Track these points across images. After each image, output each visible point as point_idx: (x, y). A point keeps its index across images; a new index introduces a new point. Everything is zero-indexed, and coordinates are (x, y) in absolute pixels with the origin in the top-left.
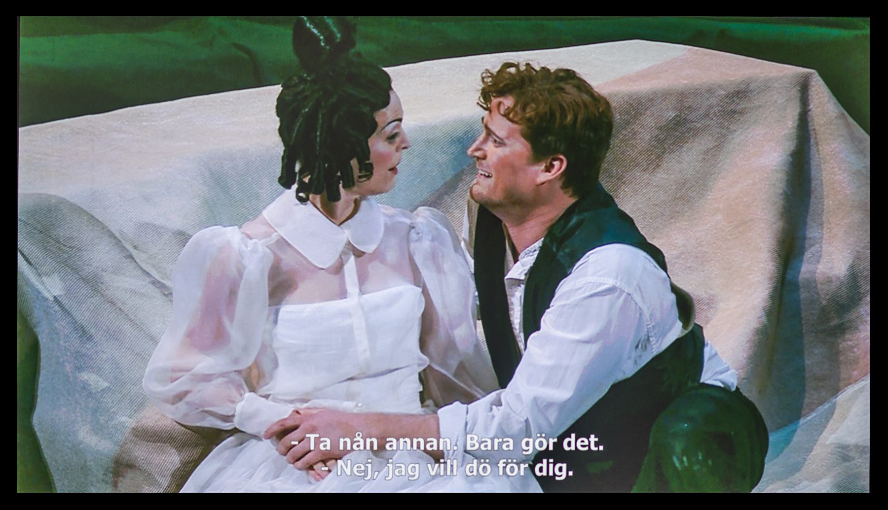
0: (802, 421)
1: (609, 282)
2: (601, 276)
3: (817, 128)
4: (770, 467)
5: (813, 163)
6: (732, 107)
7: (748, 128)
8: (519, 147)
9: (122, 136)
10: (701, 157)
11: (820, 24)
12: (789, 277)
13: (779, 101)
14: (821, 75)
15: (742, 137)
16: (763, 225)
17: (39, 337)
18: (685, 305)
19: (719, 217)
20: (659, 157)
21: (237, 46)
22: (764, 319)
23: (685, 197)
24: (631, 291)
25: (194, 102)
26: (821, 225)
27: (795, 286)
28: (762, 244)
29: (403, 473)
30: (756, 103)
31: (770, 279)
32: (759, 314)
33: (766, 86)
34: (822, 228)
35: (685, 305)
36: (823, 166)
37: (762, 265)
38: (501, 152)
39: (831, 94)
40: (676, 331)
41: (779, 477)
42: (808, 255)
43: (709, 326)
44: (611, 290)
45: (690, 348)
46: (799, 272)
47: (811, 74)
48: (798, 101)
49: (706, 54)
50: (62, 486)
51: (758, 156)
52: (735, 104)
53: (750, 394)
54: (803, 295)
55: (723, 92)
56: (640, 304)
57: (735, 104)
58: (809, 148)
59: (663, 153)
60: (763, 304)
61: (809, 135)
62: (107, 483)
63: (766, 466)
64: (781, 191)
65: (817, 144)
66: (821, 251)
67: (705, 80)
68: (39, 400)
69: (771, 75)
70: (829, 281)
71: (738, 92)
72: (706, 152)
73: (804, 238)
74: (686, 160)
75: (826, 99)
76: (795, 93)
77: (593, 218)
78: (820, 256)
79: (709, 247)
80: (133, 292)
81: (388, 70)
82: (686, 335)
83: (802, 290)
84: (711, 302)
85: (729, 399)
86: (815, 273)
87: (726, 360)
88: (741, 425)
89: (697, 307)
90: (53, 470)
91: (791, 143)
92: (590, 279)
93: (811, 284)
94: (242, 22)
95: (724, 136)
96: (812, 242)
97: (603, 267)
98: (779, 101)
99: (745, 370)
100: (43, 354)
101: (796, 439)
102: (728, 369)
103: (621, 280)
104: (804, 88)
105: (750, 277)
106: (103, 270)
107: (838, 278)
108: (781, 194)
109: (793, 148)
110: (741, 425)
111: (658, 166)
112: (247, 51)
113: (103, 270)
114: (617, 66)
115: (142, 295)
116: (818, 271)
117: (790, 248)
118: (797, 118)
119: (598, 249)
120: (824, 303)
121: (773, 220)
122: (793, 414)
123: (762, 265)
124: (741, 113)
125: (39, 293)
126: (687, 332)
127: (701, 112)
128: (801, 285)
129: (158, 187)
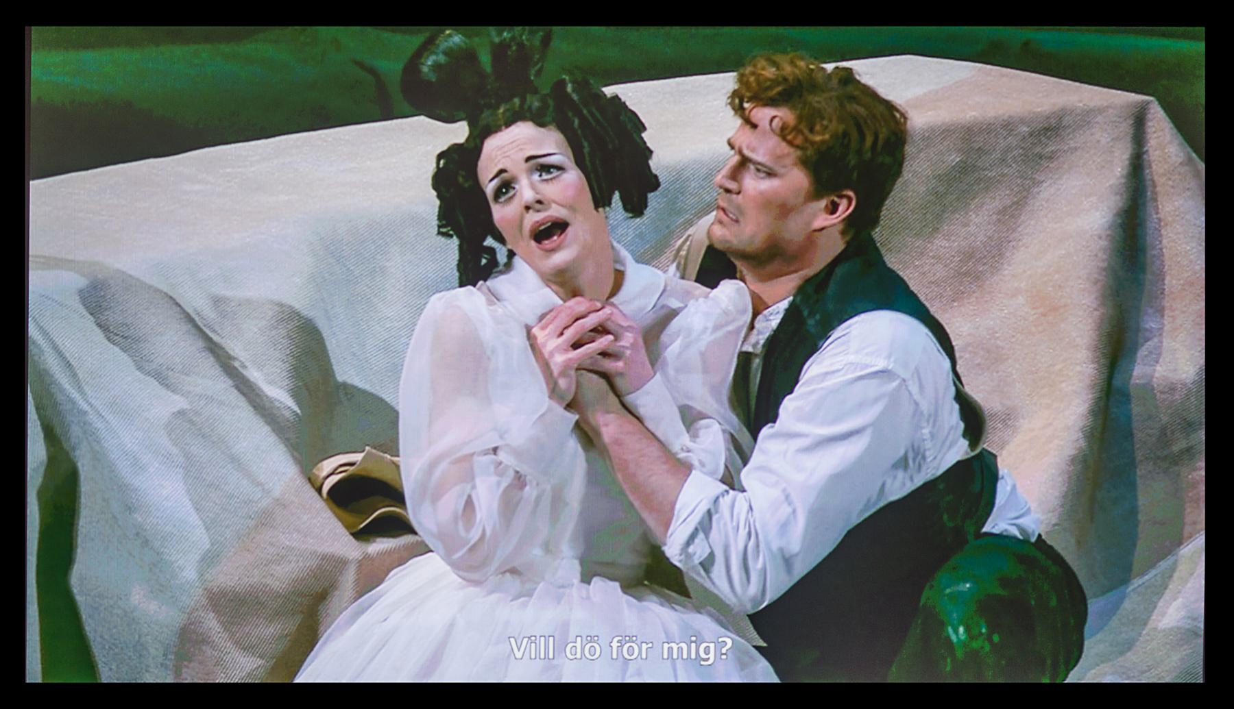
0: (1136, 582)
1: (881, 364)
2: (867, 354)
3: (1156, 178)
4: (1093, 645)
5: (1151, 225)
6: (1038, 150)
7: (1060, 178)
8: (797, 179)
9: (197, 187)
10: (995, 217)
11: (1164, 35)
12: (1117, 382)
13: (1103, 141)
14: (1160, 103)
15: (1052, 190)
16: (1081, 313)
17: (79, 465)
18: (973, 420)
19: (1021, 300)
20: (939, 218)
21: (360, 65)
22: (1082, 443)
23: (975, 269)
24: (904, 374)
25: (298, 139)
26: (1161, 311)
27: (1126, 396)
28: (1078, 339)
29: (578, 656)
30: (1072, 144)
31: (1093, 387)
32: (1075, 437)
33: (1085, 118)
34: (1163, 316)
35: (973, 420)
36: (1163, 232)
37: (1078, 368)
38: (766, 185)
39: (1175, 131)
40: (959, 450)
41: (1103, 659)
42: (1142, 352)
43: (1004, 452)
44: (883, 373)
45: (975, 480)
46: (1131, 375)
47: (1148, 103)
48: (1129, 138)
49: (1003, 75)
50: (108, 674)
51: (1073, 216)
52: (1043, 140)
53: (1064, 546)
54: (1136, 409)
55: (1025, 129)
56: (917, 397)
57: (1043, 140)
58: (1144, 204)
59: (943, 211)
60: (1080, 424)
61: (1144, 186)
62: (166, 668)
63: (1086, 643)
64: (1105, 265)
65: (1156, 200)
66: (1160, 347)
67: (1000, 112)
68: (79, 550)
69: (1092, 104)
70: (1172, 389)
71: (1047, 129)
72: (1003, 211)
73: (1138, 330)
74: (975, 223)
75: (1168, 137)
76: (1126, 127)
77: (865, 278)
78: (1160, 354)
79: (1008, 338)
80: (210, 399)
81: (634, 94)
82: (973, 457)
83: (1134, 401)
84: (1008, 418)
85: (1033, 554)
86: (1152, 377)
87: (1031, 493)
88: (1046, 591)
89: (989, 424)
90: (96, 650)
91: (1118, 197)
92: (852, 358)
93: (1148, 388)
94: (372, 33)
95: (1028, 190)
96: (1147, 334)
97: (868, 342)
98: (1103, 141)
99: (1056, 513)
100: (85, 487)
101: (1127, 605)
102: (1028, 511)
103: (895, 362)
104: (1139, 121)
105: (1064, 385)
106: (168, 369)
107: (1185, 385)
108: (1105, 269)
109: (1120, 204)
110: (1046, 591)
111: (936, 230)
112: (372, 71)
113: (168, 369)
114: (921, 85)
115: (221, 403)
116: (1157, 375)
117: (1119, 343)
118: (1127, 162)
119: (863, 316)
120: (1165, 419)
121: (1094, 306)
122: (1120, 573)
123: (1078, 368)
124: (1050, 158)
125: (74, 403)
126: (973, 454)
127: (996, 155)
128: (1132, 391)
129: (235, 258)
